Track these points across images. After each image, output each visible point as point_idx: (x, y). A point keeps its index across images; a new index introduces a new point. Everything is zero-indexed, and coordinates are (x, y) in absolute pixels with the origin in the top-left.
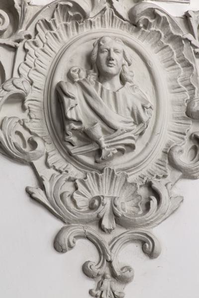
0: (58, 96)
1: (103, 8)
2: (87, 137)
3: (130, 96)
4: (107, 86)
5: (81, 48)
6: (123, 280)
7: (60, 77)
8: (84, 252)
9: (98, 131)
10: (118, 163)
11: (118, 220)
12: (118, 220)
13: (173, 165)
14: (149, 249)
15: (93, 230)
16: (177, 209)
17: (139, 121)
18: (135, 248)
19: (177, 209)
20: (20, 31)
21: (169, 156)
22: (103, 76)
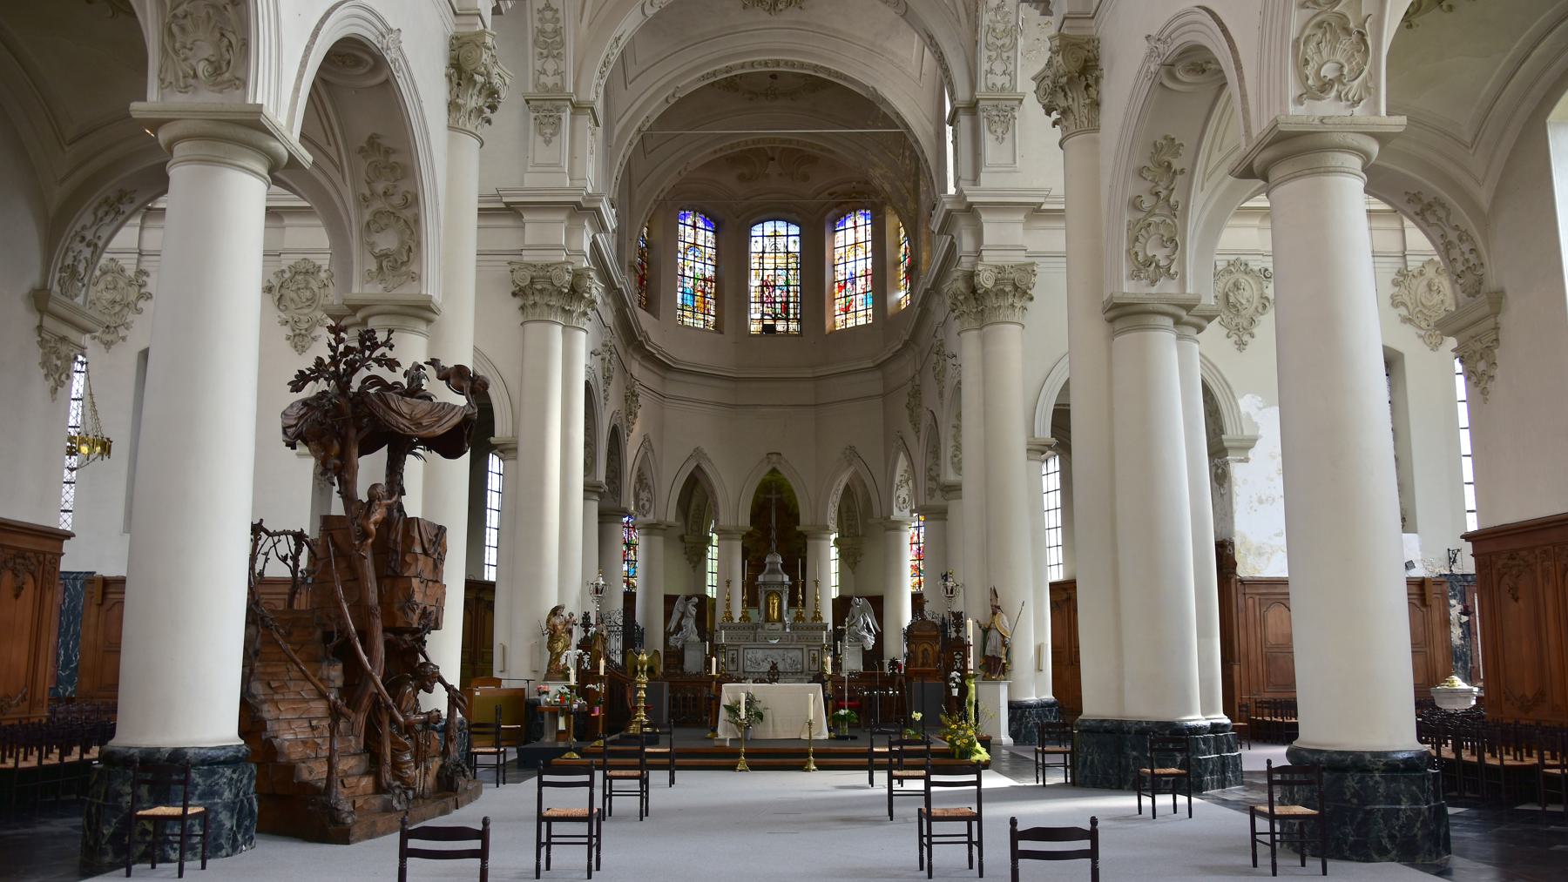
0: (1227, 296)
1: (20, 598)
2: (1234, 306)
3: (1247, 294)
4: (1240, 292)
5: (1232, 281)
6: (1246, 345)
7: (1227, 290)
8: (1235, 338)
9: (1238, 305)
10: (1244, 312)
11: (1244, 329)
12: (1244, 329)
13: (1258, 311)
14: (1252, 336)
15: (1236, 332)
16: (337, 23)
17: (1248, 301)
18: (1248, 336)
19: (337, 23)
20: (69, 529)
21: (1256, 309)
22: (1238, 289)
